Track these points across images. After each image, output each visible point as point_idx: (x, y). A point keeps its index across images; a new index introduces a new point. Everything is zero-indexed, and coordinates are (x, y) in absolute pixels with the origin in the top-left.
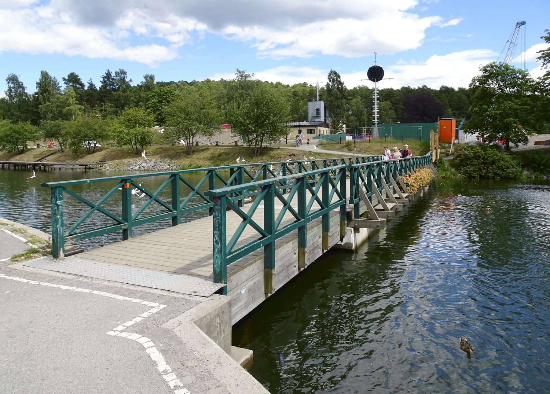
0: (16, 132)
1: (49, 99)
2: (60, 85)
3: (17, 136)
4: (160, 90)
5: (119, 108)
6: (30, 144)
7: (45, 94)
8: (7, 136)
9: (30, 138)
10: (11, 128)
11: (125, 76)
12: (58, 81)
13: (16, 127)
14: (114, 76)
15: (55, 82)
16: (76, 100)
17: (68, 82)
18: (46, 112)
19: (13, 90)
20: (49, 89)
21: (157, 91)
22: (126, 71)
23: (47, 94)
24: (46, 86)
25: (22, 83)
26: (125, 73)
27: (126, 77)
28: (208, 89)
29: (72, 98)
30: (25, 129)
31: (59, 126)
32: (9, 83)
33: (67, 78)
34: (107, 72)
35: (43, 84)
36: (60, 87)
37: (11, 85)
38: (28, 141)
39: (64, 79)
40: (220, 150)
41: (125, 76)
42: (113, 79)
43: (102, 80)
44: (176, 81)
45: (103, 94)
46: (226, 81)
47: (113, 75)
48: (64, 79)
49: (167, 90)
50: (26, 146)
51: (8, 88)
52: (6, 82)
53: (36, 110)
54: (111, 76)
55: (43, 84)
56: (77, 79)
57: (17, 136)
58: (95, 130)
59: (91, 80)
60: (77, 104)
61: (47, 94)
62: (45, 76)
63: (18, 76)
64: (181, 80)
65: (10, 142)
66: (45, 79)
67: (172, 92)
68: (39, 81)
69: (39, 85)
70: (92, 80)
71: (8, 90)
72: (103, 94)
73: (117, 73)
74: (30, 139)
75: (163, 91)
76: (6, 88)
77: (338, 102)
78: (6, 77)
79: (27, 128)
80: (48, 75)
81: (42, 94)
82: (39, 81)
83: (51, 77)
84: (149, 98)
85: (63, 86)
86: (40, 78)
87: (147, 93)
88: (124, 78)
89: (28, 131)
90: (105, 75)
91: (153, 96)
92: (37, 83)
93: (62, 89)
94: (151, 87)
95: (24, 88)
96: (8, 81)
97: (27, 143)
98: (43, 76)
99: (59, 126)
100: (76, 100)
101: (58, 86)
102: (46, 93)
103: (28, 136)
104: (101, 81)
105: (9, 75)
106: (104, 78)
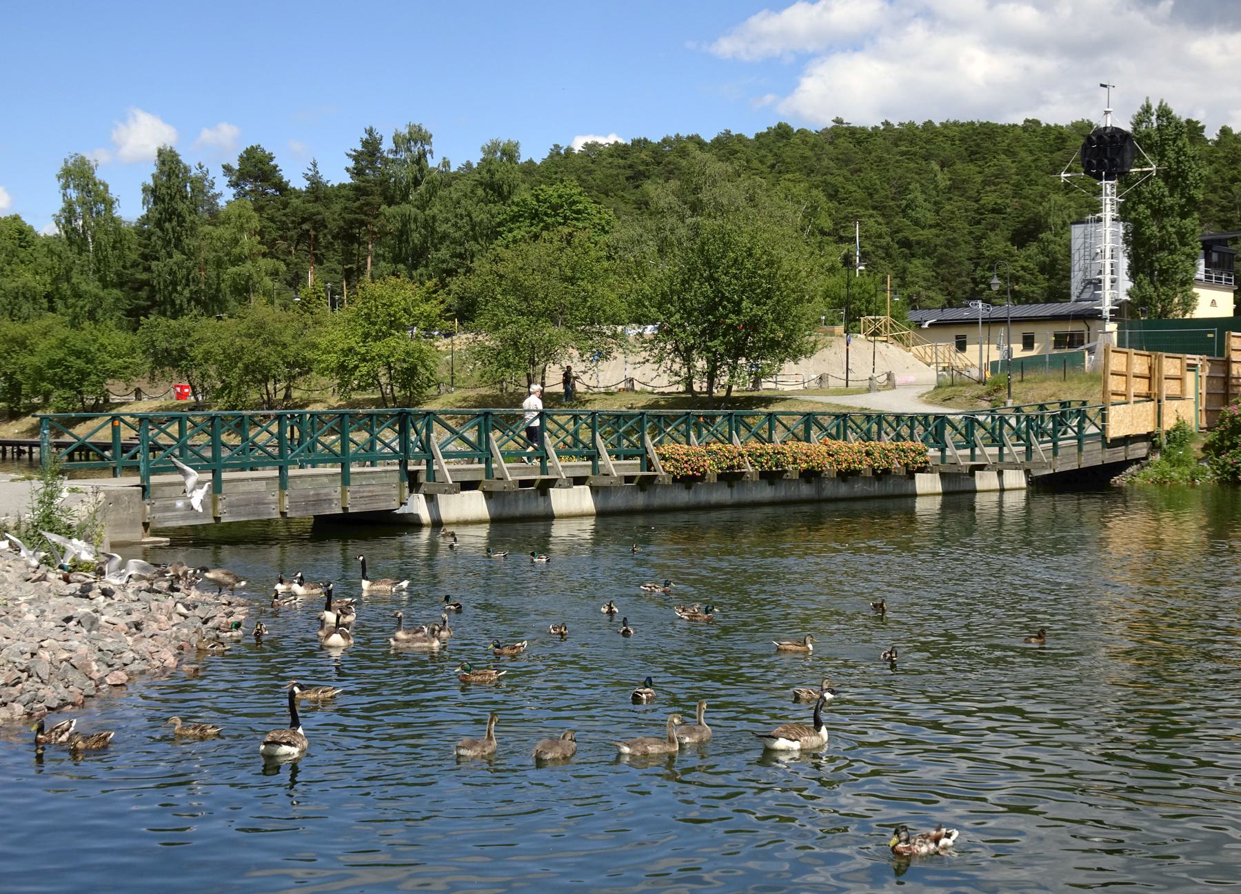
0: (78, 354)
1: (179, 239)
2: (216, 190)
3: (80, 363)
4: (537, 196)
5: (404, 261)
6: (116, 390)
7: (167, 225)
8: (52, 364)
9: (115, 372)
10: (63, 342)
11: (427, 148)
12: (210, 177)
13: (77, 339)
14: (391, 151)
15: (200, 185)
16: (259, 243)
17: (239, 179)
18: (174, 283)
19: (79, 210)
20: (181, 207)
21: (524, 201)
22: (430, 131)
23: (174, 223)
24: (172, 198)
25: (106, 187)
26: (424, 138)
27: (431, 152)
28: (773, 166)
29: (251, 235)
30: (102, 345)
31: (189, 335)
32: (66, 187)
33: (236, 166)
34: (365, 136)
35: (164, 191)
36: (216, 196)
37: (73, 194)
38: (109, 381)
39: (228, 169)
40: (621, 406)
41: (427, 148)
42: (386, 162)
43: (351, 164)
44: (656, 139)
45: (352, 216)
46: (855, 128)
47: (387, 146)
48: (228, 169)
49: (560, 197)
50: (106, 395)
51: (62, 205)
52: (57, 185)
53: (145, 276)
54: (378, 150)
55: (164, 191)
56: (266, 168)
57: (80, 363)
58: (285, 346)
59: (315, 165)
60: (264, 255)
61: (174, 223)
62: (169, 162)
63: (93, 164)
64: (673, 135)
65: (63, 385)
66: (169, 176)
67: (575, 203)
68: (151, 182)
69: (154, 194)
70: (319, 168)
71: (64, 210)
72: (352, 216)
73: (401, 142)
74: (113, 374)
75: (545, 201)
76: (58, 205)
77: (1162, 228)
78: (58, 168)
79: (106, 342)
80: (179, 162)
81: (159, 224)
82: (151, 182)
83: (187, 170)
84: (500, 224)
85: (225, 194)
86: (155, 170)
87: (495, 209)
88: (423, 155)
89: (109, 348)
90: (359, 148)
91: (515, 218)
92: (145, 190)
93: (222, 202)
94: (505, 188)
95: (110, 204)
96: (63, 181)
97: (106, 387)
98: (163, 163)
99: (189, 335)
100: (259, 243)
101: (212, 192)
102: (170, 220)
103: (108, 366)
104: (347, 170)
105: (66, 162)
106: (356, 159)
